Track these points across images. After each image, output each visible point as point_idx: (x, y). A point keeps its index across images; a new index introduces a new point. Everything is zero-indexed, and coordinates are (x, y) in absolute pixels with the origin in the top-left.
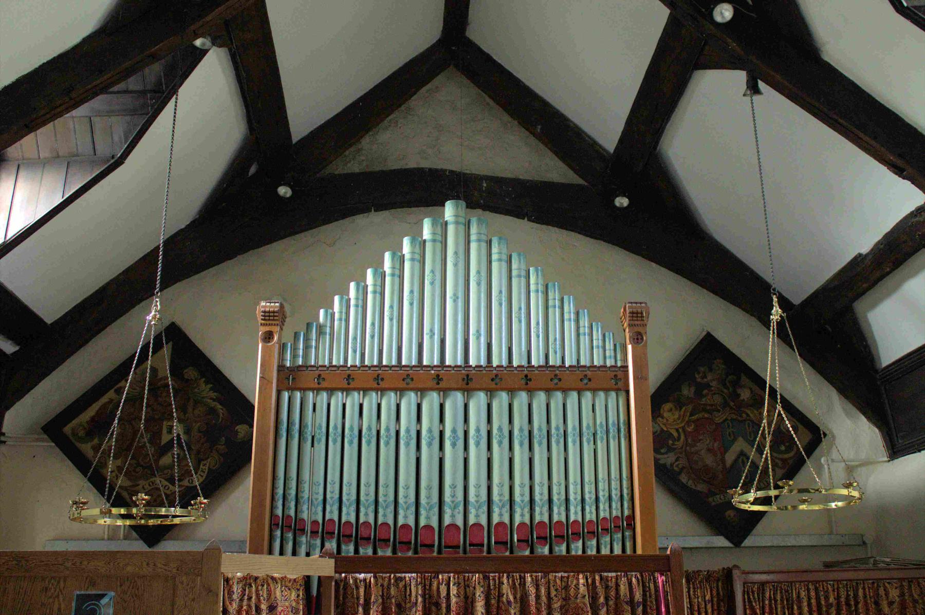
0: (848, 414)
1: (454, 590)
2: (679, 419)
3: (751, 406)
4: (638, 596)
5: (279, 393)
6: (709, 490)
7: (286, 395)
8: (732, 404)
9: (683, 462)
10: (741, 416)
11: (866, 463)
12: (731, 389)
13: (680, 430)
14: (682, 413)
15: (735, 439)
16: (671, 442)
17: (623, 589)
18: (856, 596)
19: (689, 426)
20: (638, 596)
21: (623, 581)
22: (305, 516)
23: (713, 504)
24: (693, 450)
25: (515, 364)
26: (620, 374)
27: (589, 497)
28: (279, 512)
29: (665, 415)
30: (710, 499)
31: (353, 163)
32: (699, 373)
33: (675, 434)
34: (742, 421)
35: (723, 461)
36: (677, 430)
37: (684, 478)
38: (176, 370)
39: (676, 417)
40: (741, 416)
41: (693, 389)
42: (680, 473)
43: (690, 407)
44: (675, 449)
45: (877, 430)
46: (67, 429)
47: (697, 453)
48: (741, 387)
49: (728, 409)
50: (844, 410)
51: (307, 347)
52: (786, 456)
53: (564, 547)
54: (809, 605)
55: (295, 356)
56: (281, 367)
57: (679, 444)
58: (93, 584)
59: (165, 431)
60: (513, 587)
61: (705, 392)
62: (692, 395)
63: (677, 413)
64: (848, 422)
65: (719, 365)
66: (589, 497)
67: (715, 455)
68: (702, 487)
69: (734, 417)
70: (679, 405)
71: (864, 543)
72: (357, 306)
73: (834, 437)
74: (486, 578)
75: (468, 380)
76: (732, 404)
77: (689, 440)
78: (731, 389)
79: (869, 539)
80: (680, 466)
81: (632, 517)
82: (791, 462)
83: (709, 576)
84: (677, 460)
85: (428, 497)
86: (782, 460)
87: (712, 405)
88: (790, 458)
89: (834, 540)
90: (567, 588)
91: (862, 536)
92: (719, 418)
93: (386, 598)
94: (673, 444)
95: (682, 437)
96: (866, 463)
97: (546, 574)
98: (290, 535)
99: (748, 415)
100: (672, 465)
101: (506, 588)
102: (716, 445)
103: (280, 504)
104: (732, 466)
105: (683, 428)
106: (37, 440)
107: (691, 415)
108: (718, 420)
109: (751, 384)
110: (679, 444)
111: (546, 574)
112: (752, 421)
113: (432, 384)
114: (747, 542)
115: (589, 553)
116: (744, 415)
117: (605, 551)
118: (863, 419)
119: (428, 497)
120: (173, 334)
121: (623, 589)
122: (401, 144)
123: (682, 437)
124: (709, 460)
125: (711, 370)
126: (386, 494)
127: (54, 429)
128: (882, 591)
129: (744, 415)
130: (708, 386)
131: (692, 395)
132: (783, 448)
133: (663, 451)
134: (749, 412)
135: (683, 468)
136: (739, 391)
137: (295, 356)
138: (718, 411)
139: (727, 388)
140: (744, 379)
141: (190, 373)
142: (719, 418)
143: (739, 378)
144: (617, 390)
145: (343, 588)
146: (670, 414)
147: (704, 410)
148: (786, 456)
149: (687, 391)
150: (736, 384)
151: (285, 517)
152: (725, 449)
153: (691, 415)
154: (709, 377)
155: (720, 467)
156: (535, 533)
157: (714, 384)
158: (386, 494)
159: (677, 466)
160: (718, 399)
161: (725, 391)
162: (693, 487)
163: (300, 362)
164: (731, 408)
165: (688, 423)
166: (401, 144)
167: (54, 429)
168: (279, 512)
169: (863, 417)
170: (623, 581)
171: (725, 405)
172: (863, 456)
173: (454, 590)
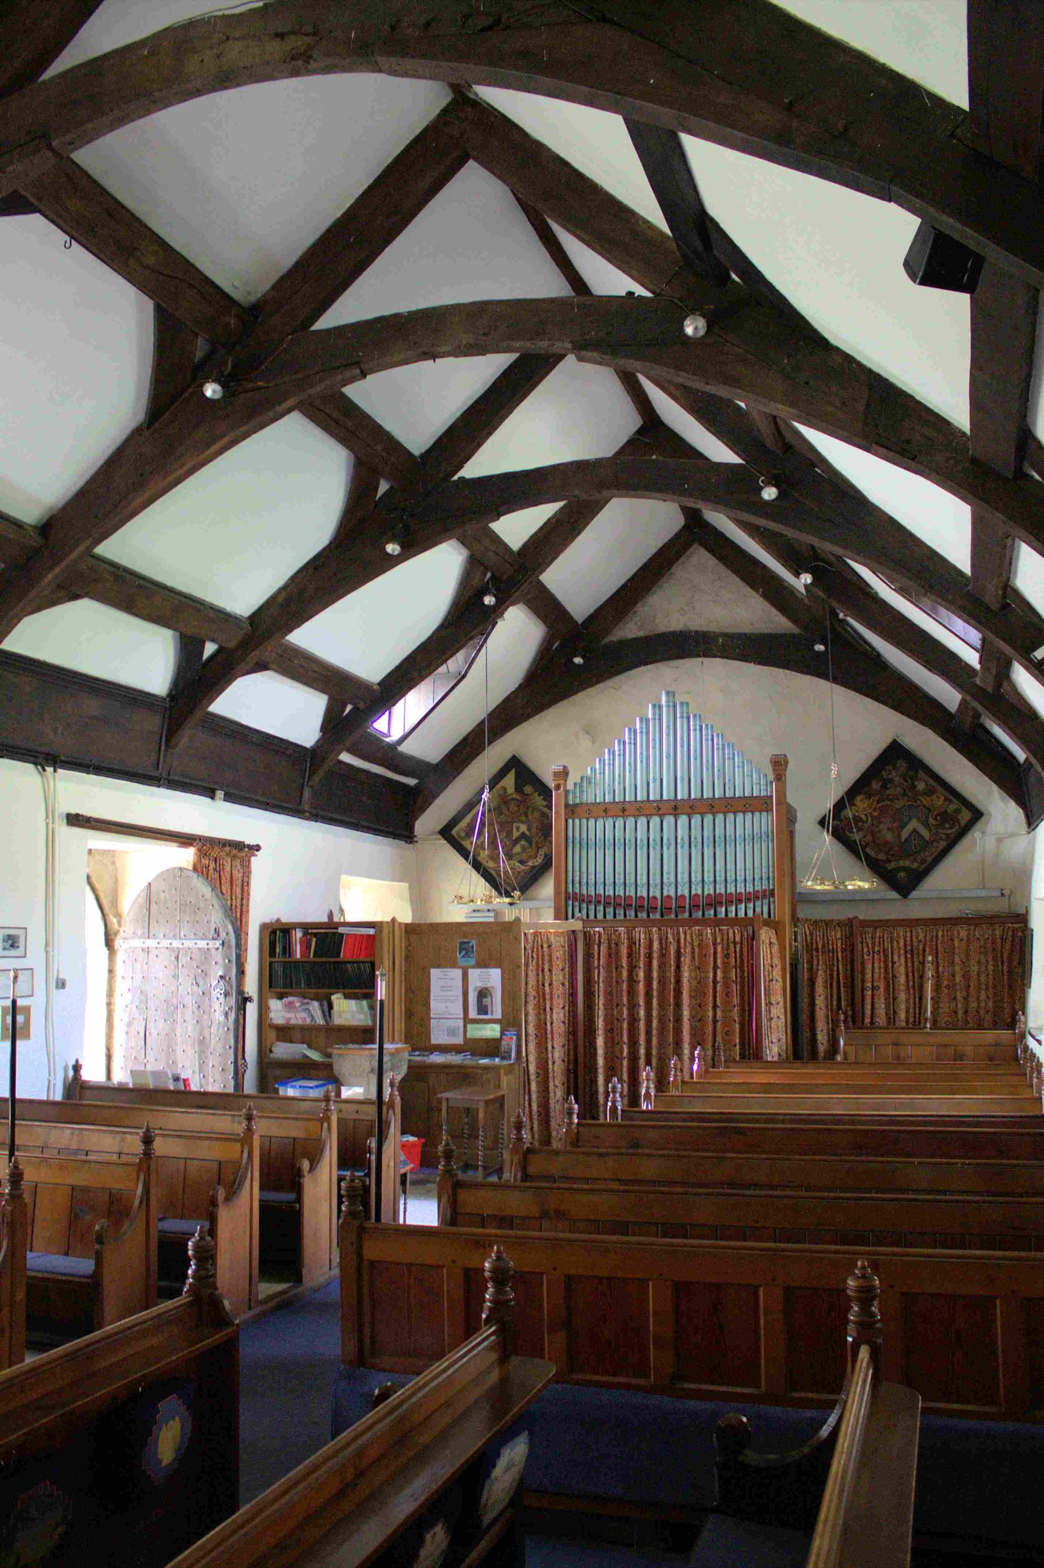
0: (1003, 799)
1: (642, 936)
4: (738, 939)
5: (566, 821)
7: (570, 821)
9: (869, 838)
11: (1012, 835)
15: (910, 819)
17: (731, 935)
18: (937, 936)
20: (738, 939)
21: (731, 931)
22: (584, 892)
26: (768, 801)
27: (749, 878)
28: (570, 890)
29: (858, 804)
31: (630, 630)
33: (864, 818)
35: (899, 835)
38: (519, 788)
41: (880, 783)
46: (454, 832)
47: (879, 832)
49: (906, 798)
50: (1001, 796)
51: (581, 792)
53: (712, 912)
54: (905, 941)
55: (575, 797)
56: (567, 805)
58: (465, 937)
59: (514, 830)
60: (673, 935)
62: (878, 788)
65: (902, 765)
66: (749, 878)
68: (882, 856)
70: (869, 796)
71: (1003, 895)
72: (641, 733)
73: (990, 814)
74: (660, 930)
75: (676, 808)
79: (1006, 892)
81: (773, 890)
82: (952, 836)
83: (839, 924)
85: (655, 879)
89: (983, 893)
90: (701, 934)
93: (609, 940)
95: (870, 820)
97: (690, 928)
98: (577, 904)
101: (670, 936)
103: (570, 886)
104: (907, 840)
106: (436, 839)
107: (878, 802)
108: (897, 806)
109: (926, 778)
111: (690, 928)
113: (654, 811)
114: (914, 894)
115: (730, 915)
117: (732, 915)
119: (655, 879)
120: (515, 764)
121: (731, 935)
122: (668, 610)
123: (870, 820)
124: (889, 837)
126: (631, 879)
127: (446, 832)
128: (956, 933)
130: (891, 780)
136: (916, 783)
137: (575, 797)
140: (921, 774)
141: (528, 789)
144: (767, 811)
145: (588, 937)
149: (875, 785)
150: (915, 778)
151: (574, 893)
156: (714, 901)
157: (897, 779)
158: (631, 879)
163: (578, 801)
166: (668, 610)
167: (446, 832)
168: (570, 890)
170: (731, 931)
171: (904, 794)
173: (642, 936)
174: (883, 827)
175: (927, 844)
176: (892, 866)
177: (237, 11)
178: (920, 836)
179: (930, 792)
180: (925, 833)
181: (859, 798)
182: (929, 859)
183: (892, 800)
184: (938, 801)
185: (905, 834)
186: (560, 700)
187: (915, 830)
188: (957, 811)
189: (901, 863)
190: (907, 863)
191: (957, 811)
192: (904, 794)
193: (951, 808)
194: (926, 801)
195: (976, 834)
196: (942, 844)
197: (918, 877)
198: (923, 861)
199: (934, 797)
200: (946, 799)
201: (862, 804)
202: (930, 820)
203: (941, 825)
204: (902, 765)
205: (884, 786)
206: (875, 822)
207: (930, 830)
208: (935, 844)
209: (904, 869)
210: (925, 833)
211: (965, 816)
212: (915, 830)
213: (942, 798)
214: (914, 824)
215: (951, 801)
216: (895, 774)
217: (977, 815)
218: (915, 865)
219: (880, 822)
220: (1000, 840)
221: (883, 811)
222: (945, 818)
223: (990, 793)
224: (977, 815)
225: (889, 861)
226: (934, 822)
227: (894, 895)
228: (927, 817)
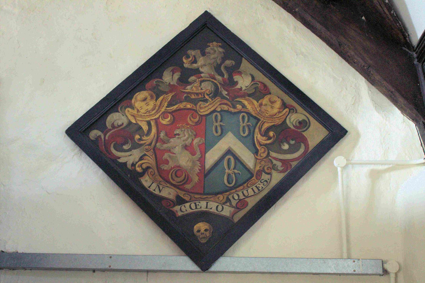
0: (378, 107)
2: (153, 110)
3: (249, 95)
6: (178, 197)
8: (225, 93)
9: (150, 161)
10: (234, 107)
11: (397, 166)
12: (226, 76)
13: (153, 123)
14: (158, 102)
16: (137, 137)
19: (165, 118)
23: (180, 214)
24: (165, 146)
25: (423, 161)
27: (212, 105)
29: (137, 105)
30: (177, 208)
32: (188, 57)
33: (145, 128)
34: (235, 113)
35: (202, 160)
36: (149, 123)
37: (146, 181)
39: (150, 107)
40: (234, 107)
41: (177, 76)
42: (142, 175)
43: (169, 97)
44: (142, 145)
45: (413, 125)
48: (240, 73)
49: (218, 99)
52: (289, 157)
57: (147, 139)
61: (192, 78)
62: (174, 82)
63: (152, 103)
64: (376, 114)
65: (215, 50)
67: (193, 153)
68: (168, 193)
69: (226, 108)
70: (157, 93)
71: (385, 272)
73: (358, 135)
76: (225, 93)
77: (162, 135)
78: (226, 76)
79: (391, 268)
80: (144, 166)
82: (294, 164)
84: (141, 158)
86: (284, 162)
87: (197, 94)
88: (293, 160)
91: (383, 263)
92: (204, 109)
94: (140, 139)
96: (397, 166)
99: (244, 106)
100: (133, 165)
102: (196, 141)
105: (157, 121)
107: (170, 104)
108: (204, 111)
110: (147, 139)
112: (249, 114)
114: (222, 264)
116: (239, 107)
118: (397, 112)
124: (184, 160)
125: (203, 54)
129: (239, 107)
130: (197, 72)
131: (174, 82)
132: (286, 147)
133: (125, 147)
134: (246, 103)
135: (148, 168)
136: (236, 78)
138: (206, 101)
139: (222, 75)
140: (245, 65)
142: (204, 109)
143: (239, 64)
146: (143, 104)
147: (188, 99)
148: (289, 157)
149: (169, 77)
150: (234, 70)
152: (205, 148)
153: (170, 104)
154: (201, 61)
155: (197, 169)
159: (141, 166)
160: (207, 87)
161: (219, 78)
162: (157, 192)
164: (223, 97)
165: (164, 115)
169: (397, 109)
171: (216, 93)
172: (392, 157)
174: (176, 144)
175: (250, 176)
176: (186, 209)
177: (137, 94)
178: (237, 159)
179: (259, 93)
180: (248, 158)
181: (140, 95)
182: (252, 202)
183: (195, 102)
184: (272, 106)
185: (212, 157)
186: (170, 237)
187: (229, 152)
188: (304, 124)
189: (202, 205)
190: (214, 206)
191: (304, 124)
192: (216, 93)
193: (293, 120)
194: (251, 106)
195: (336, 158)
196: (277, 178)
197: (229, 233)
198: (242, 204)
199: (265, 101)
200: (284, 105)
201: (143, 107)
202: (258, 136)
203: (275, 145)
204: (215, 50)
205: (184, 80)
206: (162, 135)
207: (256, 152)
208: (265, 177)
209: (204, 216)
210: (248, 158)
211: (316, 134)
212: (229, 152)
213: (278, 104)
214: (229, 141)
215: (292, 110)
216: (205, 61)
217: (336, 133)
218: (227, 211)
219: (170, 135)
220: (375, 175)
221: (178, 117)
222: (283, 133)
223: (357, 99)
224: (336, 133)
225: (180, 201)
226: (263, 140)
227: (186, 263)
228: (251, 134)
